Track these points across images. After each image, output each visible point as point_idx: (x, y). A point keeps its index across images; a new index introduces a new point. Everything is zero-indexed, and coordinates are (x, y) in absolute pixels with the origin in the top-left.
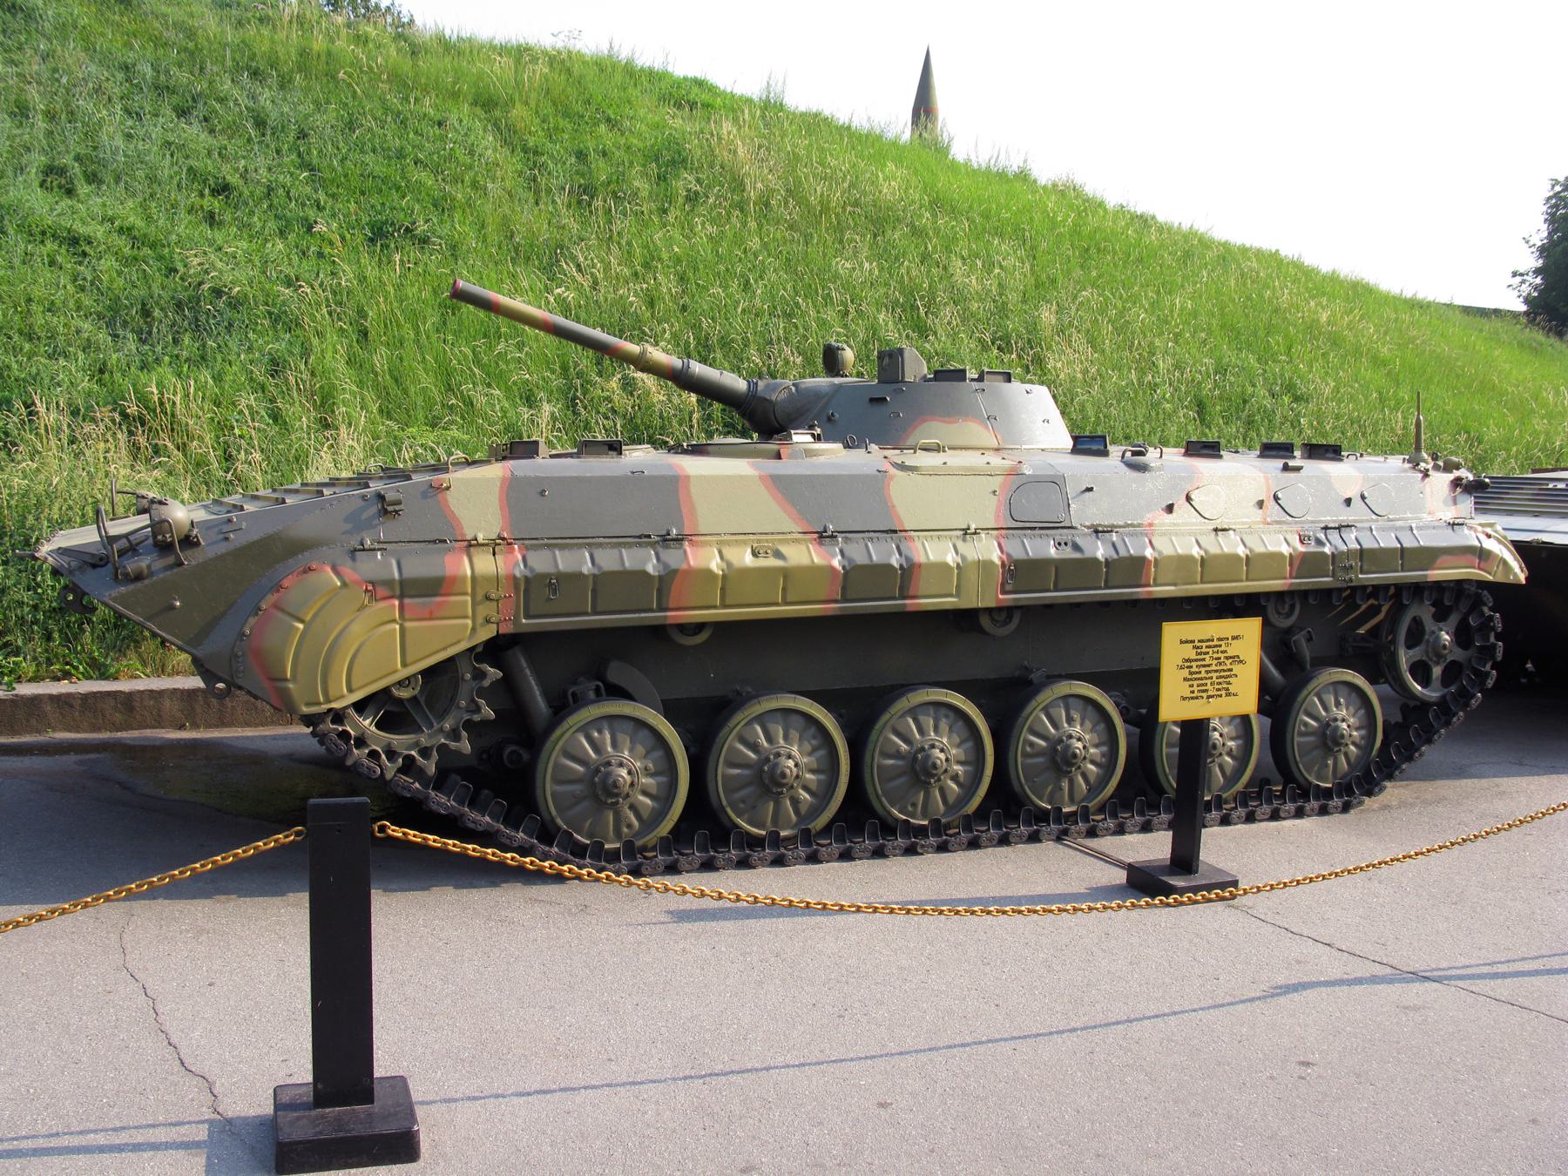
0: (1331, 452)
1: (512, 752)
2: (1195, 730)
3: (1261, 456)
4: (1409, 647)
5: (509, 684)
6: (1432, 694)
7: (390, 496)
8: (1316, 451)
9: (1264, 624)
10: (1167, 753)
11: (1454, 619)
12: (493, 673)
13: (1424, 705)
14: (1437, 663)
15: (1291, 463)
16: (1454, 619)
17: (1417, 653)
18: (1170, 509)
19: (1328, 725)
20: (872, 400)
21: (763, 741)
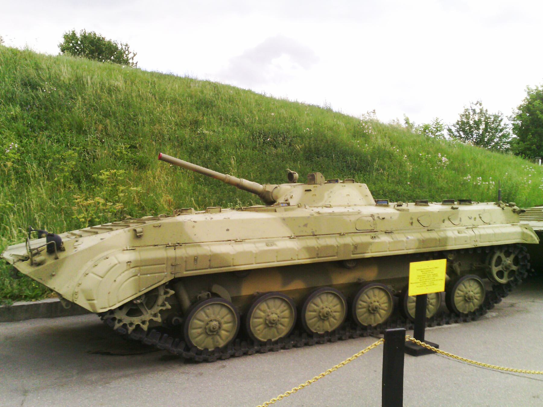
0: (468, 201)
1: (177, 319)
2: (422, 299)
3: (443, 204)
4: (496, 266)
5: (176, 296)
6: (503, 281)
7: (138, 230)
8: (462, 201)
9: (447, 261)
10: (411, 308)
11: (512, 257)
12: (172, 292)
13: (501, 285)
14: (506, 271)
15: (454, 206)
16: (512, 257)
17: (500, 268)
18: (444, 221)
19: (465, 296)
20: (306, 190)
21: (315, 307)
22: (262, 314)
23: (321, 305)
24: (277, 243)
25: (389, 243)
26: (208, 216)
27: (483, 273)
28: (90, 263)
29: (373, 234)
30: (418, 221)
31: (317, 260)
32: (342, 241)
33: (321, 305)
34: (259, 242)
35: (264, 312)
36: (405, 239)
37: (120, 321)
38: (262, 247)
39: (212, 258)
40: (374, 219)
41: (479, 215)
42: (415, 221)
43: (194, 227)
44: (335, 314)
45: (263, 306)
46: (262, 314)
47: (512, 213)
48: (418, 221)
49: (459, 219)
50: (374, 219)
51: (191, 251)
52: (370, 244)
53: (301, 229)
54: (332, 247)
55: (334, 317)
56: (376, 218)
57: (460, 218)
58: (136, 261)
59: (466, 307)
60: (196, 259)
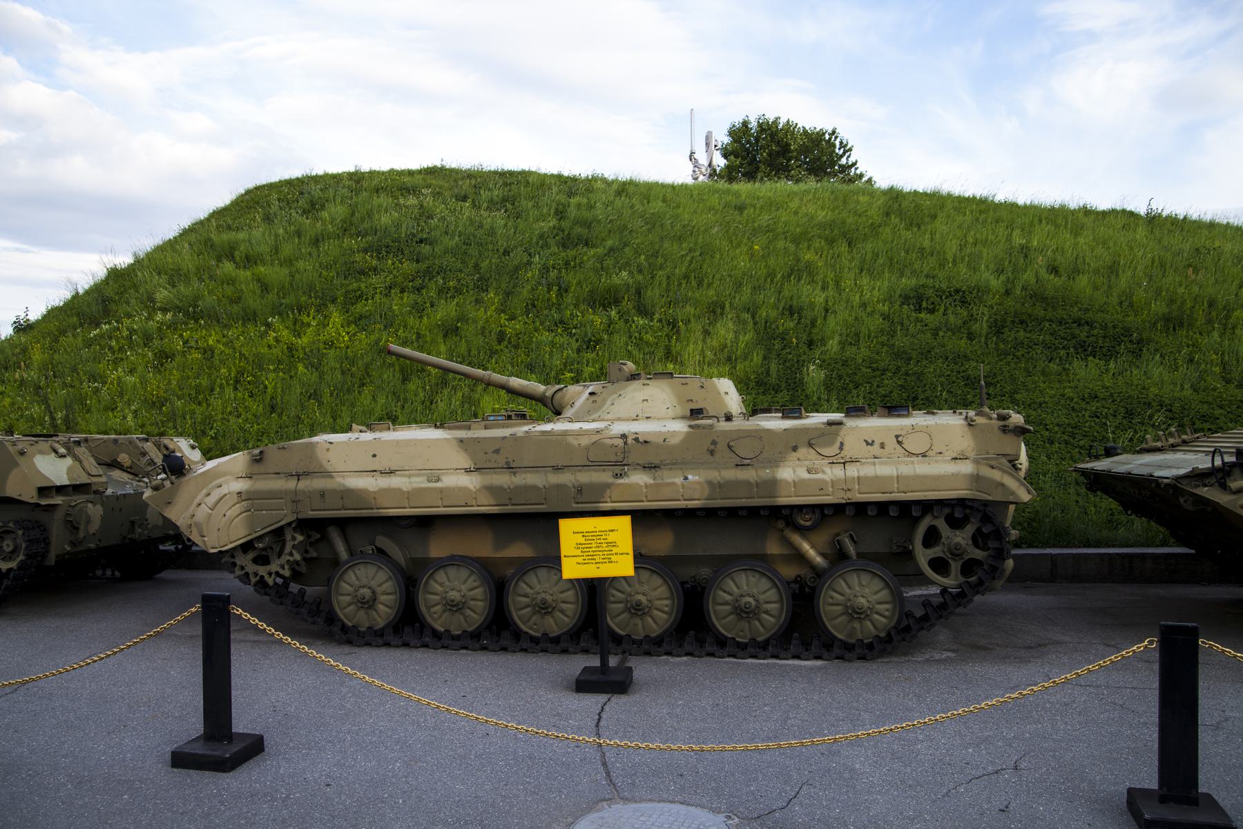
11: (970, 529)
21: (529, 590)
22: (439, 589)
23: (538, 588)
24: (443, 478)
25: (646, 486)
26: (377, 435)
27: (897, 566)
28: (204, 492)
29: (617, 470)
30: (730, 447)
31: (510, 509)
32: (554, 479)
33: (538, 588)
34: (419, 475)
35: (441, 585)
36: (679, 480)
37: (242, 568)
38: (420, 482)
39: (347, 493)
40: (625, 443)
41: (897, 437)
42: (722, 445)
43: (328, 450)
44: (564, 606)
45: (441, 576)
46: (439, 589)
47: (999, 434)
48: (730, 447)
49: (838, 444)
50: (625, 443)
51: (318, 484)
52: (609, 486)
53: (483, 459)
54: (534, 488)
55: (562, 612)
56: (630, 441)
57: (842, 444)
58: (248, 492)
59: (854, 628)
60: (323, 494)
